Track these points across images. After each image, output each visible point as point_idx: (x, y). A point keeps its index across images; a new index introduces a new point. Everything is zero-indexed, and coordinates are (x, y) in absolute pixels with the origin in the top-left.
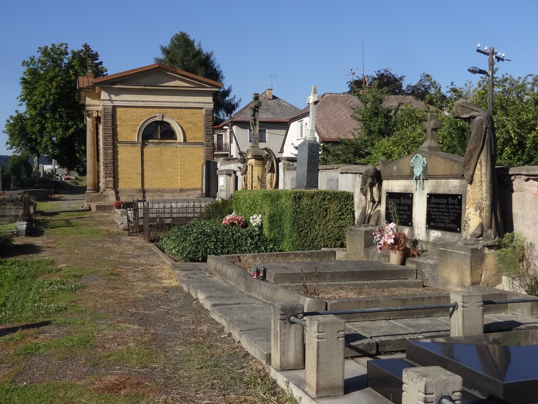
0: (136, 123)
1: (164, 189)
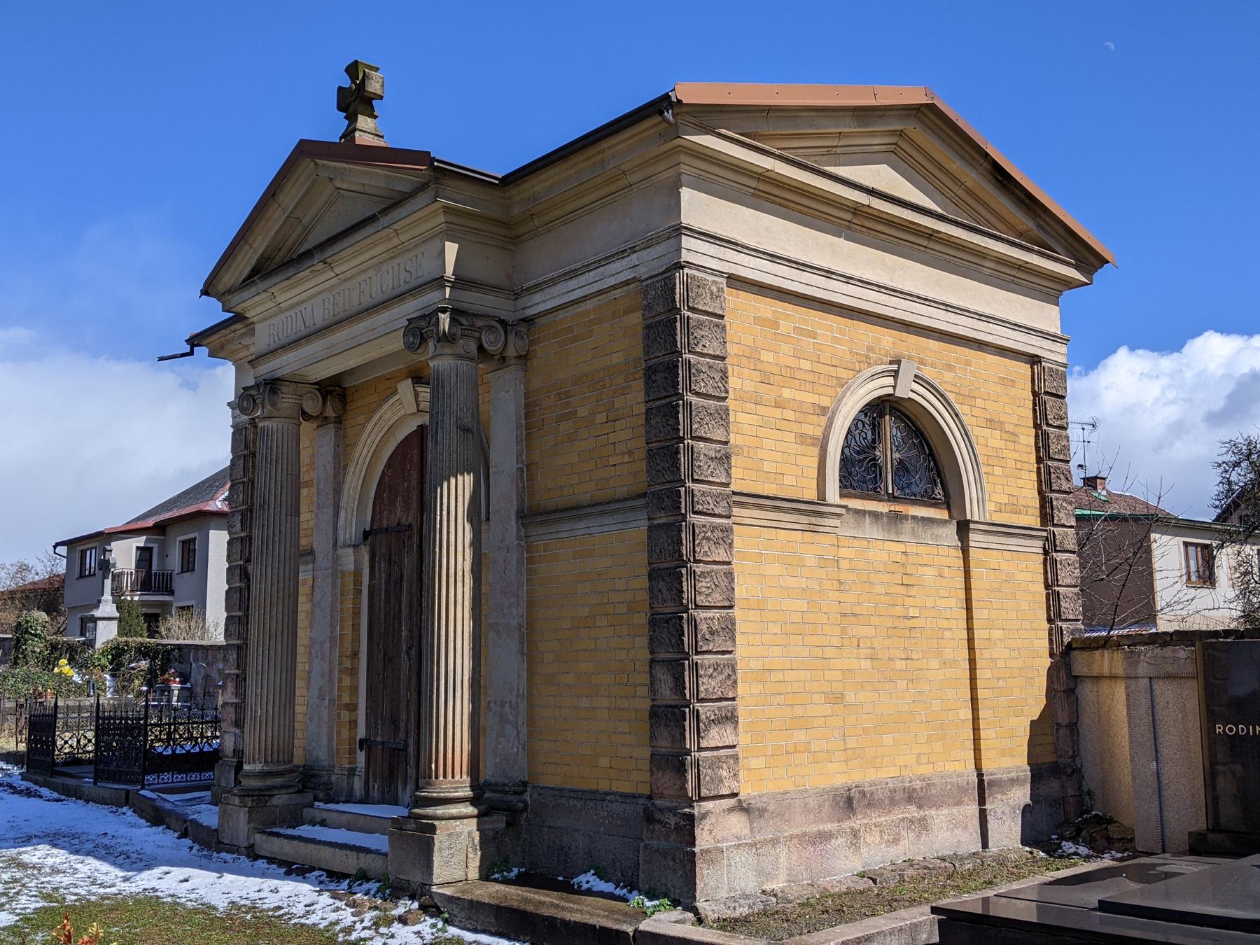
0: (814, 399)
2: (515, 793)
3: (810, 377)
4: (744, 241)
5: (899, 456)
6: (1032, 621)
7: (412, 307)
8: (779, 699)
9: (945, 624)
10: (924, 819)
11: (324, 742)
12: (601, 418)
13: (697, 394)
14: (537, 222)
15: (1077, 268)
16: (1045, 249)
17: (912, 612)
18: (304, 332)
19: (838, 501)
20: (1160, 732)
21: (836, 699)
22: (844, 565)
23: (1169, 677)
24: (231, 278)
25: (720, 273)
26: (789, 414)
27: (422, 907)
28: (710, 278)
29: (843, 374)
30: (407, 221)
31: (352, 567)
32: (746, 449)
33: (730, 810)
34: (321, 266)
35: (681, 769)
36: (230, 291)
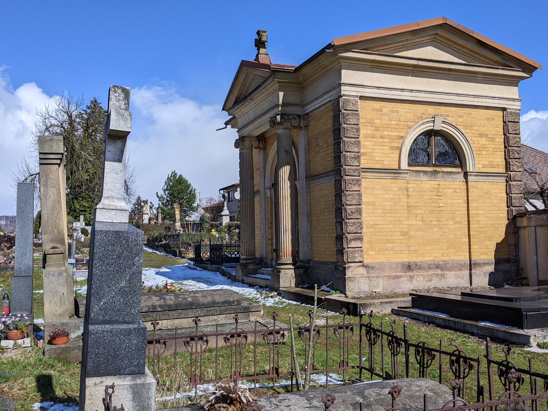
0: (398, 134)
1: (446, 263)
2: (308, 263)
3: (396, 127)
4: (366, 84)
5: (440, 151)
6: (498, 207)
7: (271, 114)
8: (381, 234)
9: (457, 209)
10: (443, 274)
11: (265, 250)
12: (325, 146)
13: (347, 137)
14: (308, 82)
15: (523, 71)
16: (505, 66)
18: (249, 121)
19: (407, 168)
20: (538, 246)
21: (404, 234)
22: (410, 190)
23: (541, 226)
24: (229, 105)
26: (387, 140)
27: (278, 294)
28: (352, 98)
29: (410, 124)
30: (270, 85)
31: (269, 195)
32: (368, 154)
33: (359, 266)
34: (250, 101)
35: (342, 254)
36: (230, 109)
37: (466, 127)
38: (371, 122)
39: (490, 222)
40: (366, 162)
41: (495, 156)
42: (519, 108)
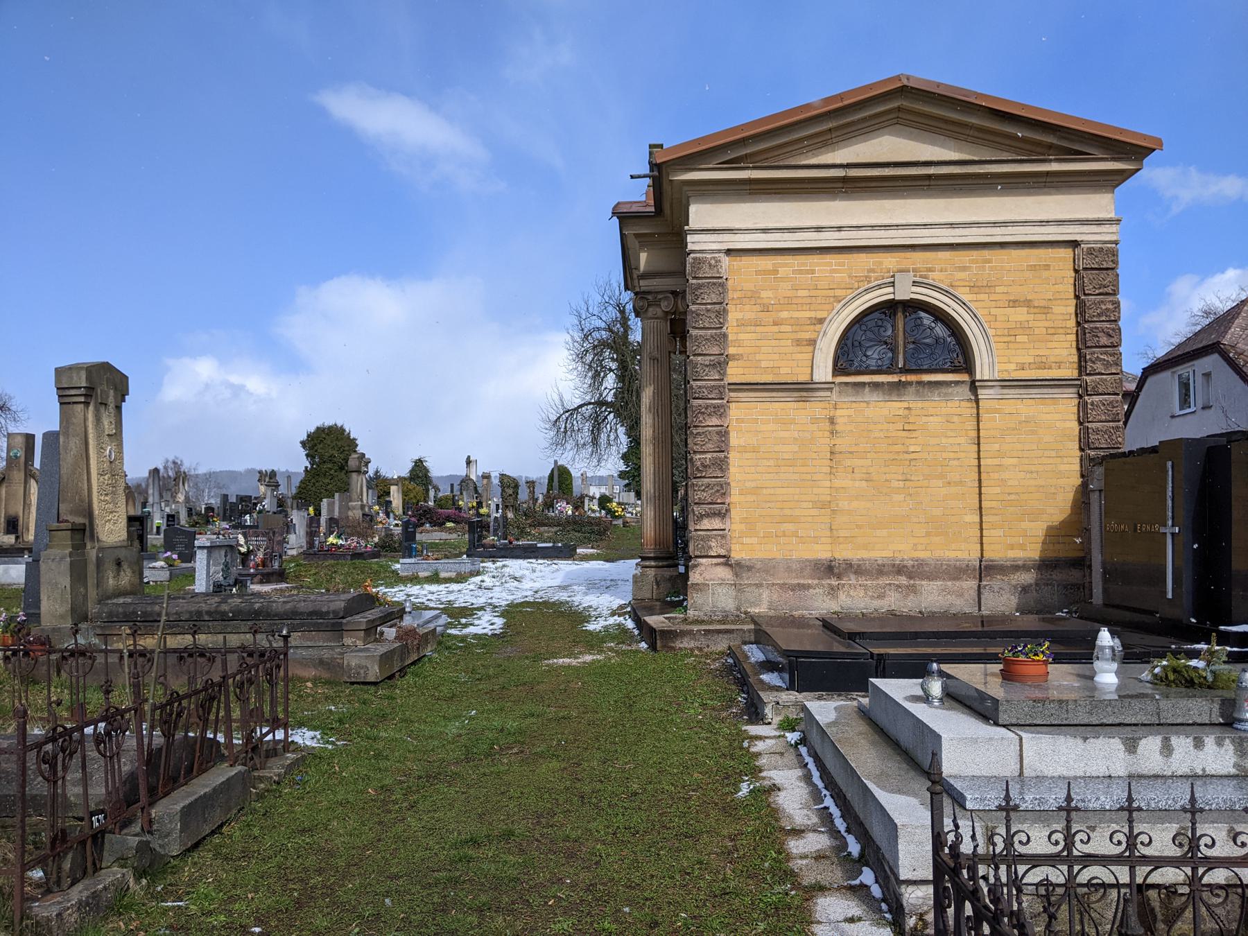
0: (813, 314)
1: (921, 563)
3: (809, 300)
4: (737, 226)
5: (905, 342)
9: (952, 455)
15: (1114, 159)
17: (912, 449)
22: (839, 420)
25: (719, 251)
26: (788, 328)
29: (839, 293)
33: (717, 564)
37: (976, 290)
38: (753, 296)
39: (1033, 482)
40: (741, 371)
41: (1050, 345)
42: (1114, 238)
